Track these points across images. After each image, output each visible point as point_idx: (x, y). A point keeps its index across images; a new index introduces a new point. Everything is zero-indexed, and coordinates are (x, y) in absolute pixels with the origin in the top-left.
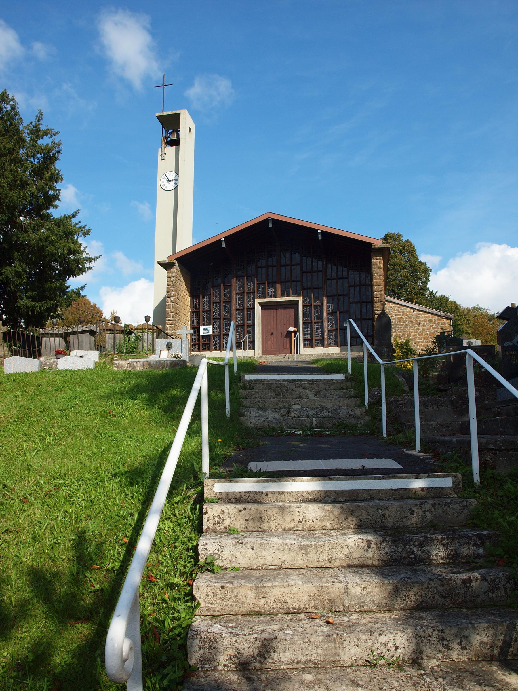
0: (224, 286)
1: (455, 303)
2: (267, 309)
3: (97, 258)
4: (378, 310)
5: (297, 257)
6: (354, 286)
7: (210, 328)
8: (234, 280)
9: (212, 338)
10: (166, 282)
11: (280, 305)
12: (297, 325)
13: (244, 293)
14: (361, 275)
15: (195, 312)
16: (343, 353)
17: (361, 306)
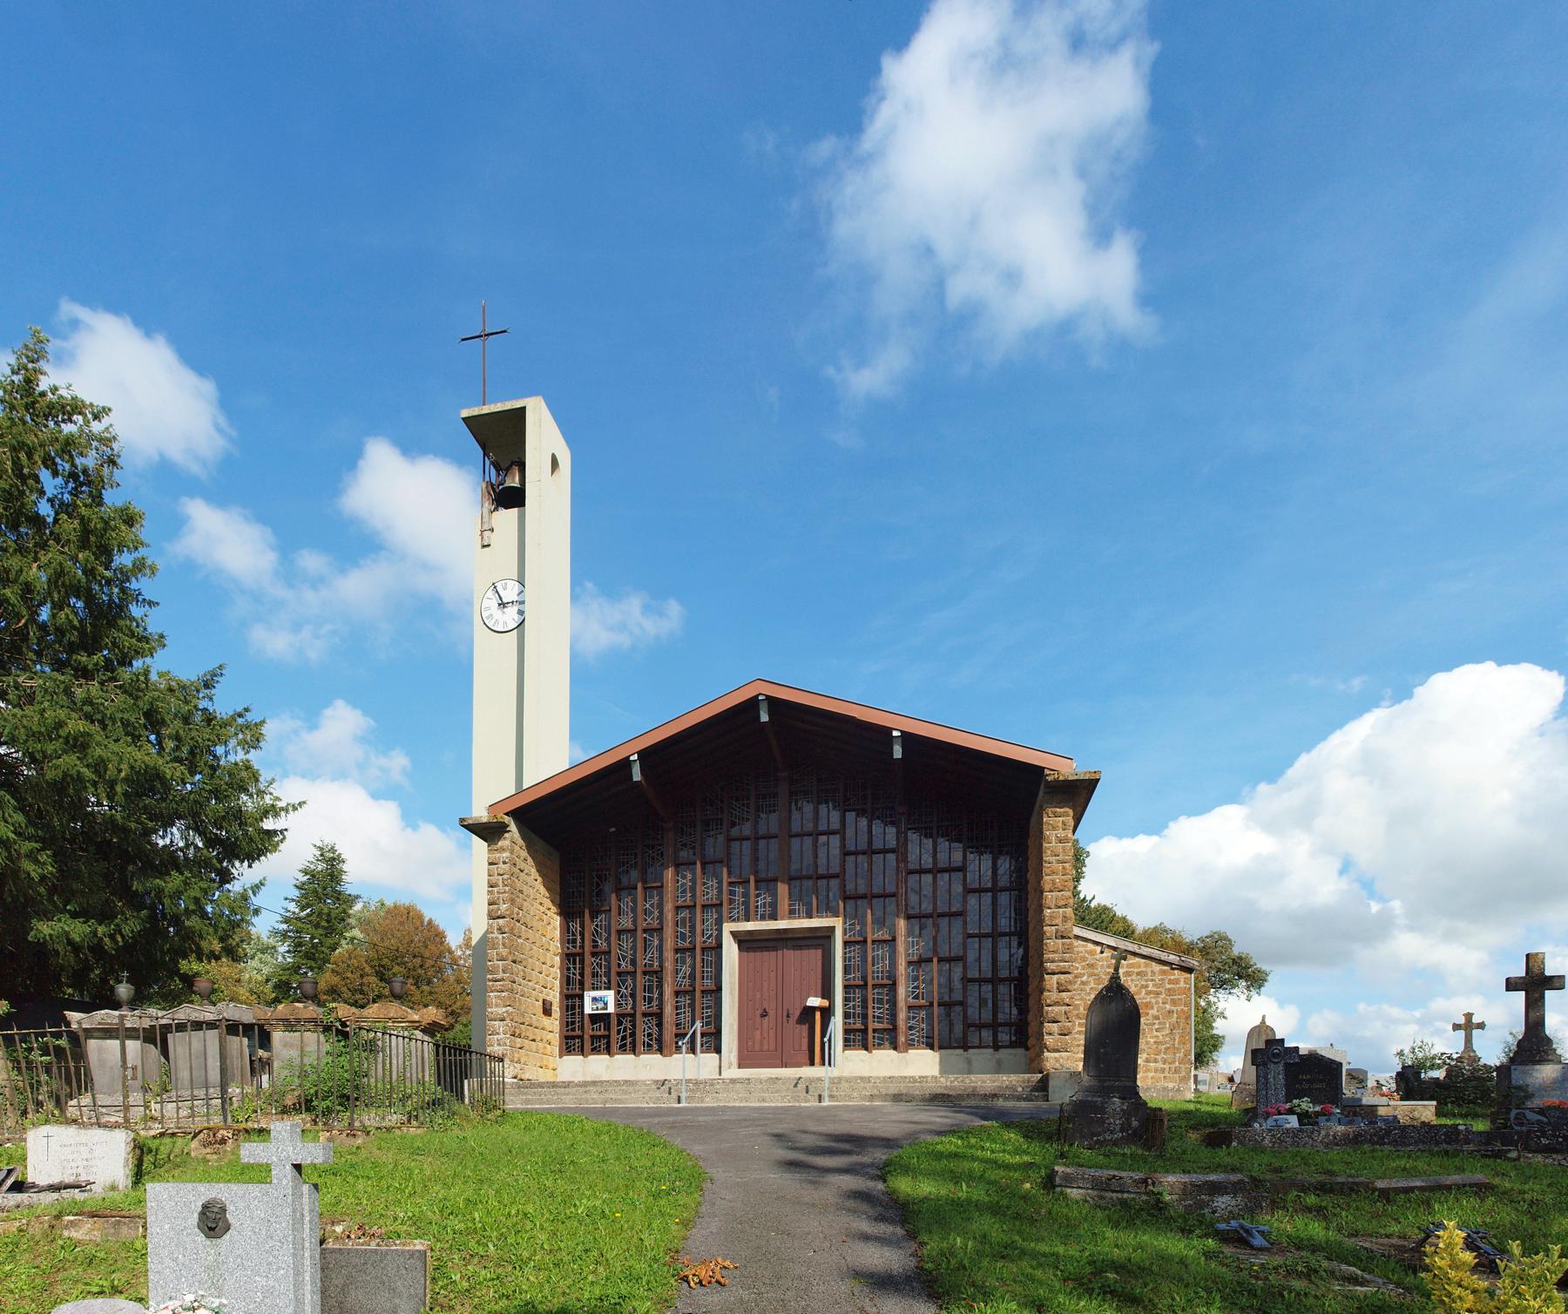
1: (1124, 919)
2: (754, 950)
3: (295, 809)
5: (831, 816)
6: (980, 891)
7: (610, 996)
8: (669, 874)
9: (614, 1022)
12: (827, 993)
14: (1000, 862)
16: (952, 1077)
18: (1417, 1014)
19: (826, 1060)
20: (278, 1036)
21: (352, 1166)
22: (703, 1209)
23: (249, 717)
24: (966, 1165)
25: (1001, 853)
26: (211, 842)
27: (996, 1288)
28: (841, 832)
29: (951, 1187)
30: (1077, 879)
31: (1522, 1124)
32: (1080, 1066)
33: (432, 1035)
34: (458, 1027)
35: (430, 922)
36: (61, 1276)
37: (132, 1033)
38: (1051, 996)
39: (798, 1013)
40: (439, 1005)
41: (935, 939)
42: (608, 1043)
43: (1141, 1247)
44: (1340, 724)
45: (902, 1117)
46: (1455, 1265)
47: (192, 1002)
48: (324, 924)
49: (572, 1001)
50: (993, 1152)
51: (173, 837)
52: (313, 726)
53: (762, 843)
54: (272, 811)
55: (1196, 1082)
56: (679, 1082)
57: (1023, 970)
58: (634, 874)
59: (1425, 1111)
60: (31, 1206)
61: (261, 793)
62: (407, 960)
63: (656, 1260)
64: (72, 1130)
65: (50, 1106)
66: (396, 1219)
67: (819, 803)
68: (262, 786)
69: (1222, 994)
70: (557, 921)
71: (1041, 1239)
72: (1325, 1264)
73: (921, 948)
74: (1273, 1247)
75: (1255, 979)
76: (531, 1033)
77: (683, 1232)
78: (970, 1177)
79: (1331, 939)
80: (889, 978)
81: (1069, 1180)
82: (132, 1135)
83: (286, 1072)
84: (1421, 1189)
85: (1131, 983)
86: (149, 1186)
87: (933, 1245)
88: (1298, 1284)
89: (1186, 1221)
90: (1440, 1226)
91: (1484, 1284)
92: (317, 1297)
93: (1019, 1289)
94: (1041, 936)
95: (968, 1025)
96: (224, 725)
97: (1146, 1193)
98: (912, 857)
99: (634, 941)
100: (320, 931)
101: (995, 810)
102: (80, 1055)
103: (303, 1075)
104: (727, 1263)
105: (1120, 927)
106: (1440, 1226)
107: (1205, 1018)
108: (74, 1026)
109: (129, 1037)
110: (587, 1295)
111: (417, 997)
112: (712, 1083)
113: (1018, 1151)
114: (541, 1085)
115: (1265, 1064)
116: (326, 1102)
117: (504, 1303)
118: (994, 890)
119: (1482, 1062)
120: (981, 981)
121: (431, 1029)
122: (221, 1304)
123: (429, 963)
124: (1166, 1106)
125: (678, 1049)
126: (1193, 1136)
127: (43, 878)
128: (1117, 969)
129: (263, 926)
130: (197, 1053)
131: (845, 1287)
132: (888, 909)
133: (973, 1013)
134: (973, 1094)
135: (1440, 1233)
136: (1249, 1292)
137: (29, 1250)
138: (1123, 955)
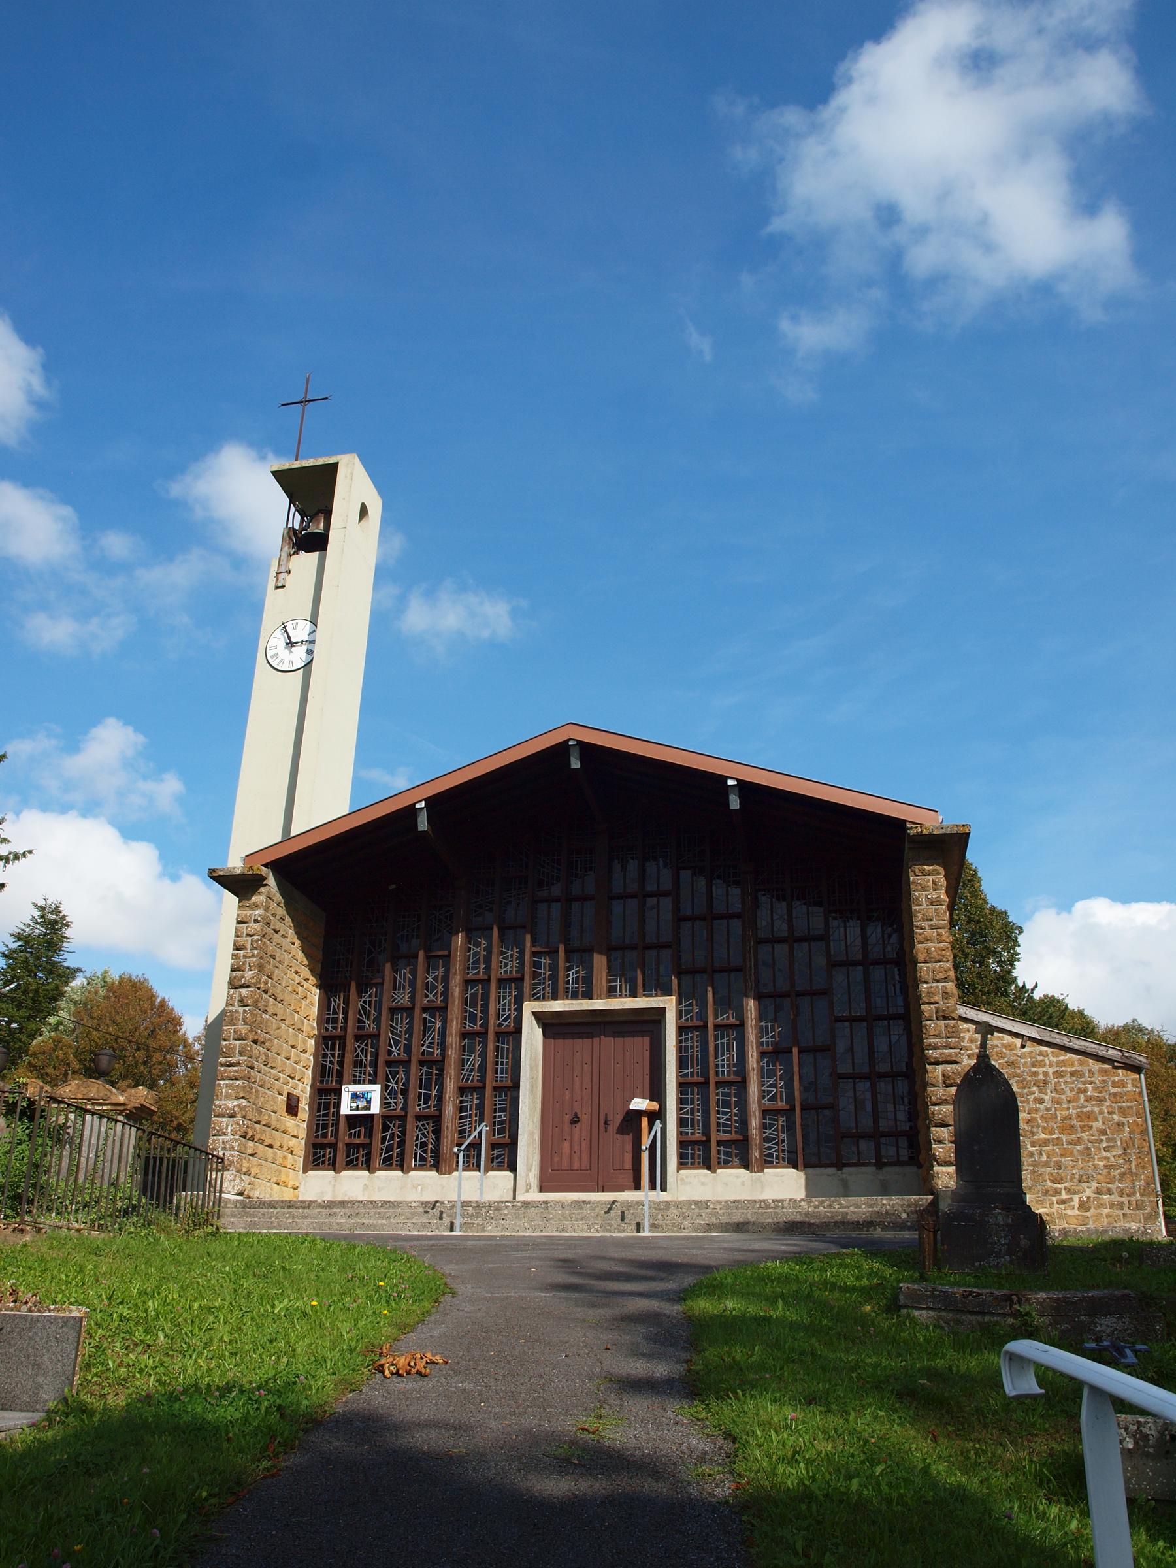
0: (428, 958)
1: (1081, 1013)
2: (563, 1036)
3: (16, 857)
4: (935, 1048)
5: (660, 875)
6: (849, 964)
7: (374, 1091)
8: (459, 940)
9: (378, 1126)
10: (233, 938)
11: (606, 1023)
12: (657, 1092)
13: (489, 980)
14: (869, 930)
15: (333, 1038)
16: (816, 1201)
17: (870, 1030)
19: (659, 1182)
35: (163, 1001)
39: (618, 1119)
42: (369, 1154)
49: (325, 1095)
53: (576, 906)
70: (315, 995)
80: (736, 1073)
98: (763, 923)
99: (411, 1023)
112: (498, 1206)
114: (272, 1205)
120: (855, 1077)
123: (158, 1056)
134: (844, 1224)
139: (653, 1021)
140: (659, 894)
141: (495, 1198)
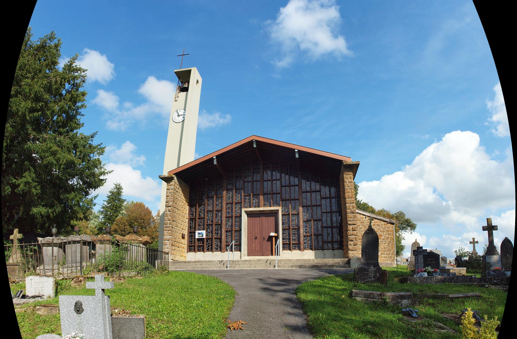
2: (252, 217)
3: (110, 173)
7: (204, 232)
8: (225, 193)
9: (205, 241)
12: (277, 231)
14: (331, 189)
15: (193, 219)
16: (319, 260)
18: (460, 238)
20: (98, 246)
21: (120, 290)
22: (235, 304)
23: (102, 146)
24: (323, 289)
25: (331, 186)
26: (84, 183)
27: (332, 331)
28: (280, 180)
29: (318, 296)
30: (356, 194)
31: (489, 275)
32: (360, 256)
33: (146, 245)
34: (154, 243)
36: (37, 326)
37: (55, 245)
38: (350, 232)
40: (148, 235)
41: (312, 213)
42: (203, 248)
43: (379, 317)
44: (425, 148)
45: (302, 273)
46: (469, 323)
47: (73, 234)
48: (114, 209)
49: (191, 234)
50: (332, 285)
51: (74, 181)
52: (119, 148)
53: (255, 183)
54: (103, 173)
55: (397, 261)
56: (227, 261)
57: (341, 224)
58: (213, 193)
59: (463, 271)
60: (27, 303)
61: (101, 168)
62: (139, 221)
63: (219, 321)
64: (37, 278)
65: (32, 269)
66: (134, 307)
67: (273, 171)
68: (101, 166)
69: (403, 232)
70: (188, 208)
71: (347, 314)
72: (434, 322)
73: (307, 216)
74: (419, 317)
75: (413, 227)
76: (178, 245)
77: (229, 312)
78: (325, 293)
79: (434, 213)
80: (297, 226)
81: (357, 294)
82: (54, 279)
83: (100, 258)
84: (462, 297)
85: (375, 228)
86: (60, 296)
87: (312, 316)
88: (425, 329)
89: (393, 308)
90: (466, 310)
91: (477, 329)
92: (111, 334)
93: (340, 331)
94: (346, 213)
95: (324, 242)
96: (94, 148)
97: (381, 299)
98: (303, 187)
99: (213, 214)
100: (113, 211)
101: (329, 174)
102: (41, 252)
103: (105, 259)
104: (243, 322)
105: (370, 210)
106: (466, 310)
107: (399, 240)
108: (40, 242)
109: (54, 246)
110: (197, 333)
111: (141, 233)
112: (238, 261)
113: (340, 285)
114: (181, 262)
115: (417, 255)
116: (112, 268)
117: (170, 335)
118: (330, 198)
119: (478, 254)
120: (327, 227)
121: (145, 243)
122: (83, 336)
123: (146, 221)
124: (388, 269)
125: (227, 250)
126: (396, 279)
127: (37, 194)
128: (370, 223)
129: (96, 209)
130: (74, 251)
131: (283, 330)
132: (296, 204)
133: (325, 238)
134: (326, 265)
135: (466, 312)
136: (411, 332)
137: (28, 318)
138: (372, 219)
139: (275, 214)
140: (276, 180)
141: (237, 259)
